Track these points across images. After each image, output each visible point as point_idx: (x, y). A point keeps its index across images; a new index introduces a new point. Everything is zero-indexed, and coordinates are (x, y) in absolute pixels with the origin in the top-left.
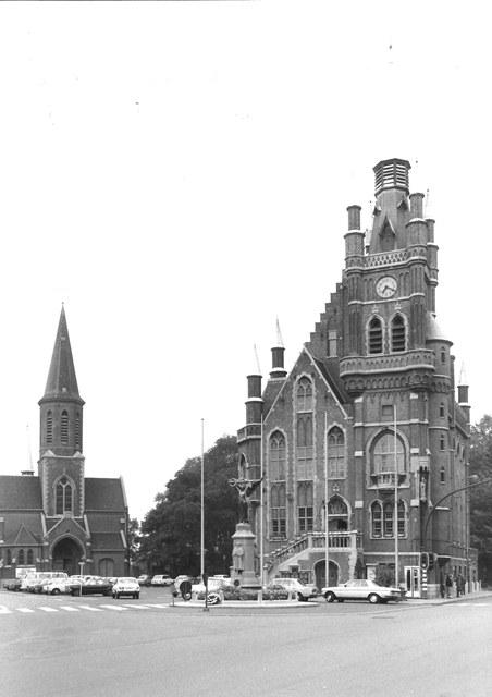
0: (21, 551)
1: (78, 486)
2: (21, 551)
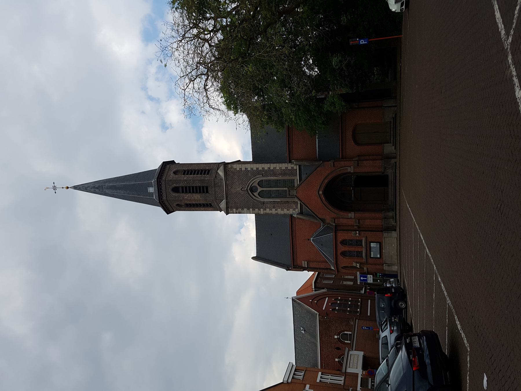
0: (343, 254)
1: (258, 172)
2: (343, 254)
